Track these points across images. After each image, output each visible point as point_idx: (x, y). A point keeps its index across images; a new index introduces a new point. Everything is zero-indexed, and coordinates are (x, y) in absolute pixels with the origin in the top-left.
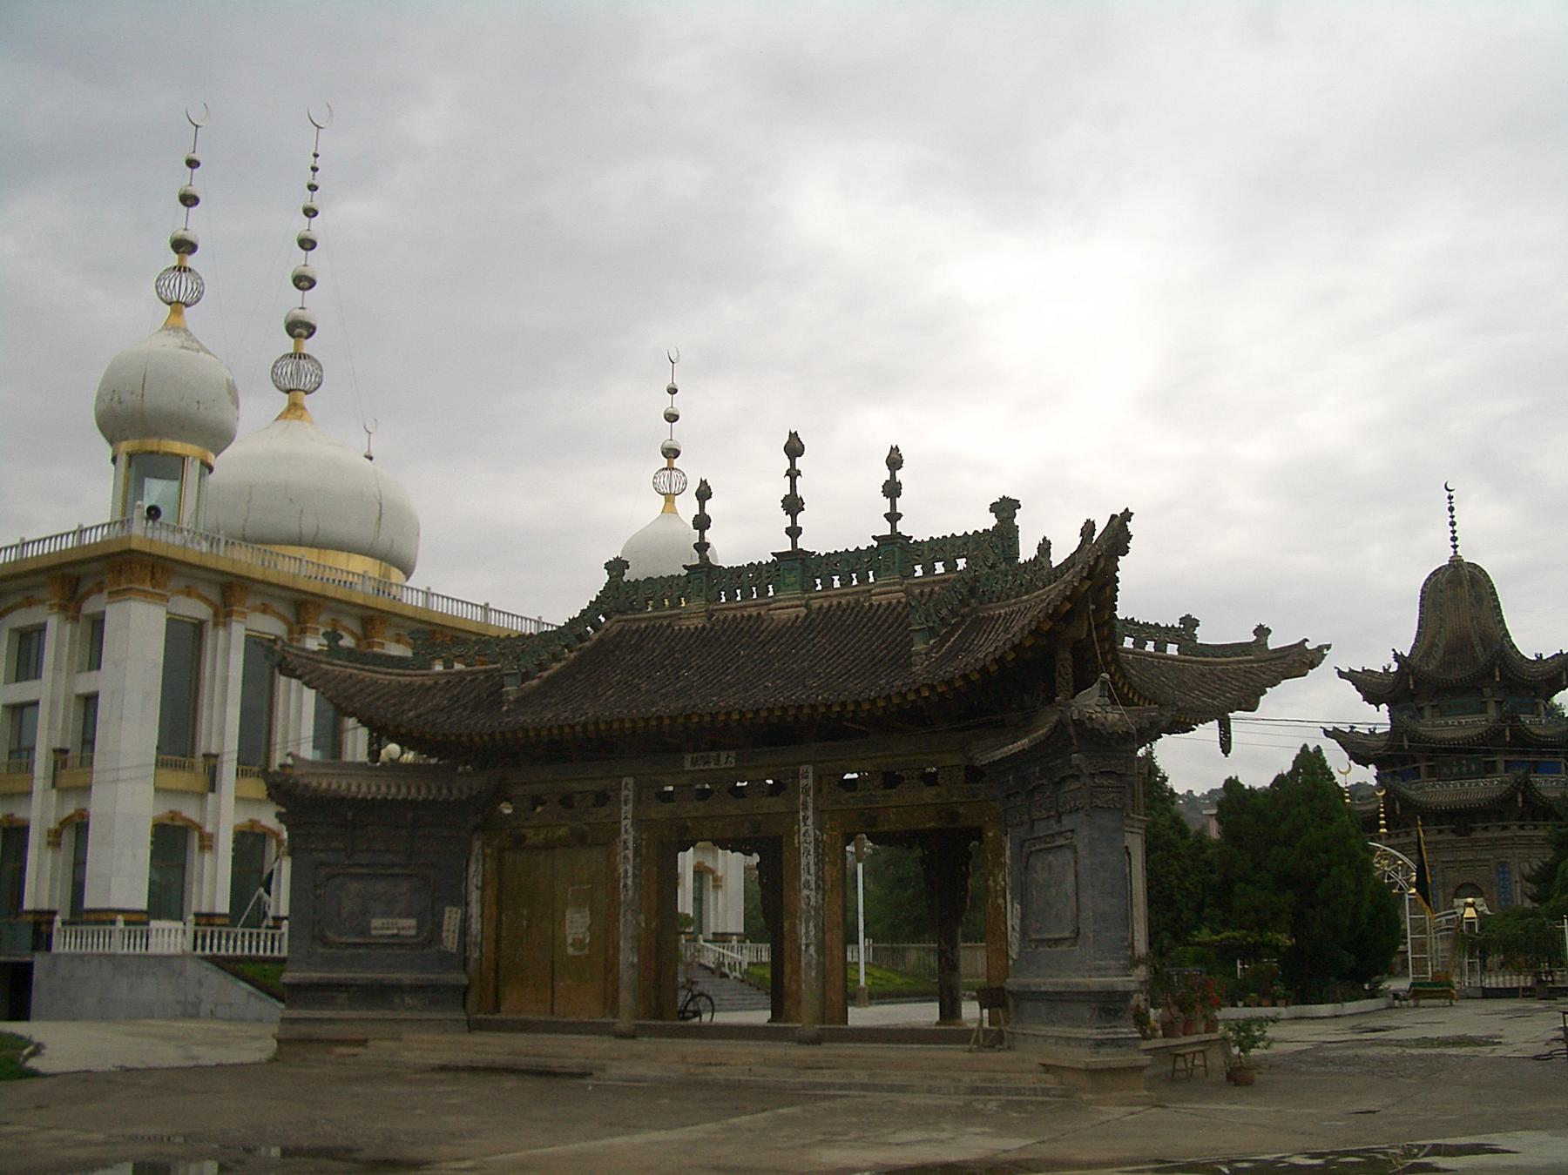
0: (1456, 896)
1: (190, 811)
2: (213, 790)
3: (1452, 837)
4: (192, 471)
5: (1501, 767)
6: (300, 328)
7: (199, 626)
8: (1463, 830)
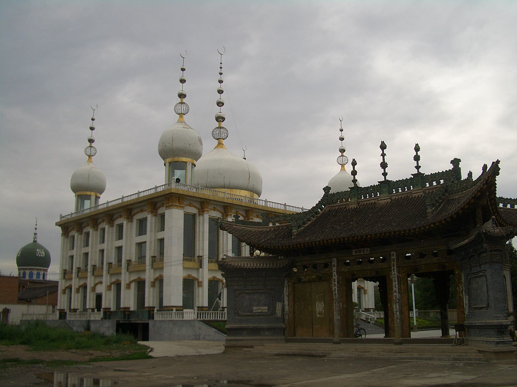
1: (194, 274)
2: (201, 268)
4: (189, 167)
6: (220, 119)
7: (194, 215)
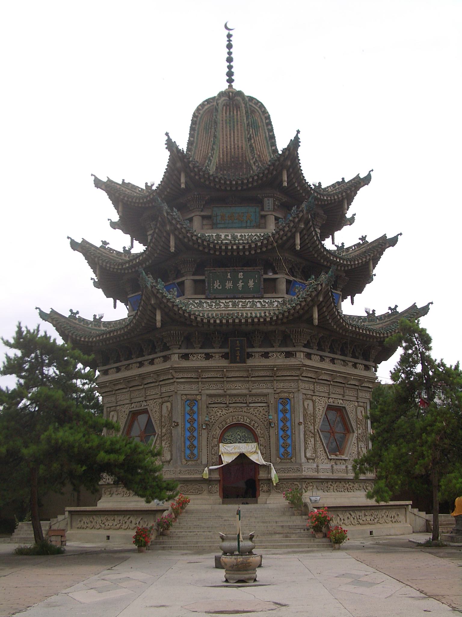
0: (222, 439)
3: (224, 363)
5: (283, 286)
8: (236, 356)
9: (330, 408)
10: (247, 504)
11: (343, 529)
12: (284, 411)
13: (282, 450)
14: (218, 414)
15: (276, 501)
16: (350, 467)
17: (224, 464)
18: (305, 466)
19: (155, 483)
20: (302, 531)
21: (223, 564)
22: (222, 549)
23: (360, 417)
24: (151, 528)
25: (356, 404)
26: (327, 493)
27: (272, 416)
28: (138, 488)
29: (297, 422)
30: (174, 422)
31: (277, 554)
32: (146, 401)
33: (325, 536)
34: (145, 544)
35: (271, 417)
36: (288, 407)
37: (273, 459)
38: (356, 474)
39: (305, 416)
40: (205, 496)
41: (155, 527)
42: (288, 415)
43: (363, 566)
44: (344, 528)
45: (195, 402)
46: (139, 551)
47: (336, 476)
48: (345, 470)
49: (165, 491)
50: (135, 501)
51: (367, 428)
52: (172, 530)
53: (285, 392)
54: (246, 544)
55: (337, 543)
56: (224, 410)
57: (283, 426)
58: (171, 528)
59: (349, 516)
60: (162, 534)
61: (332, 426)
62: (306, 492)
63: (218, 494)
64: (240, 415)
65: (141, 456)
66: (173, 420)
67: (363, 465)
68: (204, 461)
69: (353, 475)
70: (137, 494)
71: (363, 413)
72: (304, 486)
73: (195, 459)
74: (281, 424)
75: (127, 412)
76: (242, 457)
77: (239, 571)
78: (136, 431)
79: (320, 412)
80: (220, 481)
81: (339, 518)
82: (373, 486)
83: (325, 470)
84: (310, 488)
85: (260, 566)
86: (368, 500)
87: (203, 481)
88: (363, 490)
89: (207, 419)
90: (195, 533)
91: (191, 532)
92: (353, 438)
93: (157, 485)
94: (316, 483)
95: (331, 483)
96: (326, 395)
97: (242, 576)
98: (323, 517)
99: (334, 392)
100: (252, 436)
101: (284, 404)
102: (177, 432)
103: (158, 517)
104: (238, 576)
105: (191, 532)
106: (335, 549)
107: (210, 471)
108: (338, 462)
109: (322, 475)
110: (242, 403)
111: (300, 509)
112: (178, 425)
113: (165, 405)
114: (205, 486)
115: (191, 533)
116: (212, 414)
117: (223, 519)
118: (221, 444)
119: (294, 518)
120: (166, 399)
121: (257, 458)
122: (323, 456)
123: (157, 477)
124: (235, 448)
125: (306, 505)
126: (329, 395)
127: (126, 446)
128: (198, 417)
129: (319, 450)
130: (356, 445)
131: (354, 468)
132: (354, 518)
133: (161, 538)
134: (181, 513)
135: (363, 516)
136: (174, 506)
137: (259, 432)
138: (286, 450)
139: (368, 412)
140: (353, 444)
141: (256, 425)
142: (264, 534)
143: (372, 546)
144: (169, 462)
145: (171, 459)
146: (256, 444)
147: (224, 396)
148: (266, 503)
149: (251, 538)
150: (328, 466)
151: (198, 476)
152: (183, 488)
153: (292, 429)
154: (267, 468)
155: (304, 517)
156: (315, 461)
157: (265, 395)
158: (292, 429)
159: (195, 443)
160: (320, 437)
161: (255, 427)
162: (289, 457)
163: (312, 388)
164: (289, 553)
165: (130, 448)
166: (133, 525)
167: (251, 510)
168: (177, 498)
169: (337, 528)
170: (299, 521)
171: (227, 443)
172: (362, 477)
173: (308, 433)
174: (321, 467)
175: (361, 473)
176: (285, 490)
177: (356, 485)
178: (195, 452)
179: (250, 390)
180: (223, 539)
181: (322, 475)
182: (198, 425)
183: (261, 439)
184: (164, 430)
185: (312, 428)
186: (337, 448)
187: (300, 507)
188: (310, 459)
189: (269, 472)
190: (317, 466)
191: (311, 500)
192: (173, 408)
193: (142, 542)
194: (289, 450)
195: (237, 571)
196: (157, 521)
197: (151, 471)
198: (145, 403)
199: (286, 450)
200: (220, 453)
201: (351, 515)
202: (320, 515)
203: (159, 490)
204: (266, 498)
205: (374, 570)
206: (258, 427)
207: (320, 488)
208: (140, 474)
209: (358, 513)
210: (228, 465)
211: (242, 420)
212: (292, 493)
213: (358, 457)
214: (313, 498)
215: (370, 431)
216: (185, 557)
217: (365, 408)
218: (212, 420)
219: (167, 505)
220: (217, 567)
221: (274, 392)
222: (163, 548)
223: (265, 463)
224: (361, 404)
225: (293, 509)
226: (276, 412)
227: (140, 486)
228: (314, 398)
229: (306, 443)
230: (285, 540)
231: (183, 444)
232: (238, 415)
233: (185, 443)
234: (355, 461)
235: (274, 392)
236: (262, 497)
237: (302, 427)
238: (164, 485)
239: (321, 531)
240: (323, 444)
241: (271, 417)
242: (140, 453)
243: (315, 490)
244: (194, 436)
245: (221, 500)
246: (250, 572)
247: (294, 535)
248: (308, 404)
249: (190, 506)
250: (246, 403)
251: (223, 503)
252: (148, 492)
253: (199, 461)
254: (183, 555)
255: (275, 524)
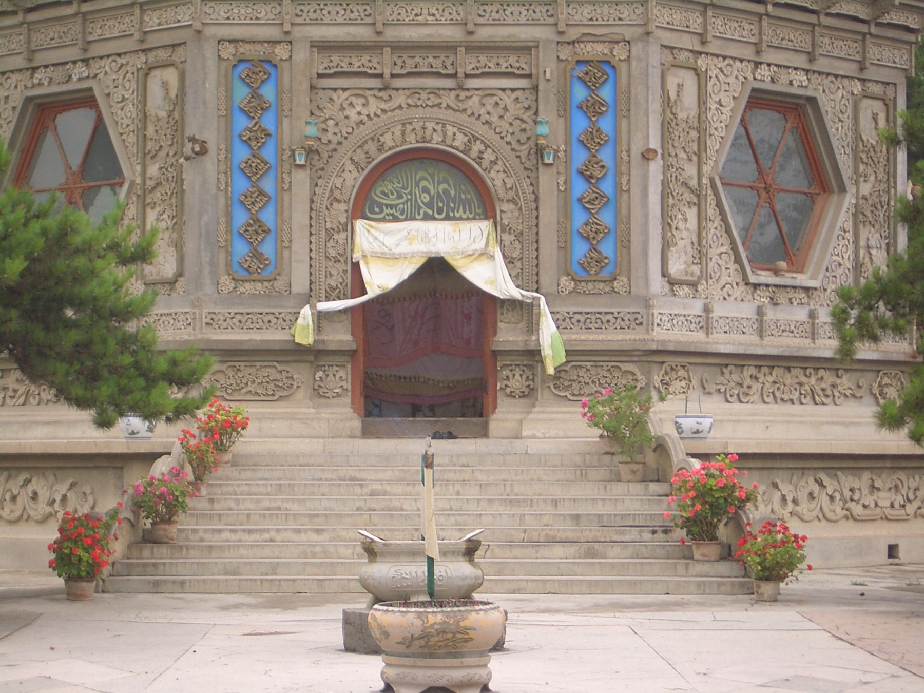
0: (364, 205)
9: (759, 100)
10: (451, 436)
11: (792, 531)
12: (593, 108)
13: (580, 249)
14: (352, 113)
15: (547, 432)
16: (824, 316)
17: (372, 292)
18: (663, 308)
19: (127, 359)
20: (647, 536)
21: (376, 633)
22: (370, 592)
23: (870, 135)
24: (114, 515)
25: (857, 88)
26: (737, 406)
27: (549, 127)
28: (67, 374)
29: (636, 151)
30: (192, 139)
31: (557, 611)
32: (85, 61)
33: (727, 554)
34: (92, 572)
35: (542, 130)
36: (606, 93)
37: (547, 280)
38: (843, 339)
39: (666, 128)
40: (301, 406)
41: (126, 514)
42: (606, 124)
43: (859, 656)
44: (796, 527)
45: (268, 67)
46: (72, 596)
47: (773, 345)
48: (802, 324)
49: (163, 385)
50: (48, 423)
51: (891, 176)
52: (183, 522)
53: (597, 39)
54: (455, 571)
55: (767, 579)
56: (372, 100)
57: (589, 164)
58: (181, 517)
59: (816, 488)
60: (149, 539)
61: (765, 164)
62: (662, 399)
63: (348, 400)
64: (430, 119)
65: (80, 262)
66: (189, 132)
67: (870, 308)
68: (300, 284)
69: (835, 343)
70: (65, 395)
71: (882, 123)
72: (657, 379)
73: (266, 274)
74: (580, 157)
75: (17, 100)
76: (436, 269)
77: (432, 656)
78: (50, 171)
79: (724, 117)
80: (353, 353)
81: (777, 496)
82: (907, 384)
83: (735, 325)
84: (677, 385)
85: (499, 647)
86: (885, 432)
87: (296, 353)
88: (868, 399)
89: (312, 131)
90: (266, 536)
91: (250, 531)
92: (839, 214)
93: (136, 365)
94: (700, 369)
95: (752, 371)
96: (748, 52)
97: (440, 673)
98: (723, 489)
99: (776, 42)
100: (475, 196)
101: (591, 83)
102: (201, 178)
103: (135, 478)
104: (430, 673)
105: (250, 531)
106: (761, 600)
107: (321, 318)
108: (782, 297)
109: (723, 342)
110: (438, 75)
111: (639, 458)
112: (204, 151)
113: (156, 77)
114: (300, 373)
115: (256, 536)
116: (328, 113)
117: (366, 490)
118: (360, 224)
119: (618, 489)
120: (162, 55)
121: (490, 276)
122: (728, 273)
123: (134, 338)
124: (409, 238)
125: (661, 447)
126: (758, 52)
127: (25, 225)
128: (279, 123)
129: (713, 252)
130: (849, 236)
131: (840, 318)
132: (832, 498)
133: (146, 553)
134: (216, 464)
135: (865, 491)
136: (193, 442)
137: (499, 183)
138: (594, 248)
139: (900, 121)
140: (837, 232)
141: (489, 156)
142: (510, 544)
143: (894, 594)
144: (171, 283)
145: (179, 274)
146: (485, 226)
147: (375, 47)
148: (518, 437)
149: (471, 550)
150: (747, 310)
151: (274, 336)
152: (220, 377)
153: (618, 174)
154: (525, 312)
155: (654, 487)
156: (693, 287)
157: (526, 49)
158: (618, 174)
159: (268, 217)
160: (719, 205)
161: (485, 163)
162: (604, 274)
163: (696, 27)
164: (597, 608)
165: (44, 232)
166: (42, 508)
167: (463, 460)
168: (201, 414)
169: (769, 526)
170: (635, 500)
171: (383, 220)
172: (865, 351)
173: (676, 189)
174: (719, 311)
175: (862, 337)
176: (587, 390)
177: (846, 382)
178: (268, 249)
179: (471, 27)
180: (371, 552)
181: (724, 342)
182: (280, 151)
183: (506, 207)
184: (153, 170)
185: (691, 170)
186: (779, 247)
187: (641, 452)
188: (681, 283)
189: (533, 326)
190: (707, 309)
191: (678, 427)
192: (189, 90)
193: (80, 564)
194: (607, 248)
195: (424, 656)
196: (131, 491)
197: (113, 314)
198: (80, 70)
199: (594, 248)
200: (357, 256)
201: (821, 485)
202: (712, 482)
203: (141, 382)
204: (519, 416)
205: (895, 670)
206: (494, 163)
207: (712, 387)
208: (74, 325)
209: (848, 481)
210: (386, 299)
211: (437, 138)
212: (612, 400)
213: (856, 281)
214: (688, 424)
215: (905, 188)
216: (235, 617)
217: (889, 105)
218: (330, 136)
219: (165, 435)
220: (349, 648)
221: (558, 38)
222: (156, 588)
223: (516, 293)
224: (877, 89)
225: (617, 458)
226: (564, 110)
227: (77, 366)
228: (702, 62)
229: (667, 223)
230: (586, 563)
231: (223, 220)
232: (425, 119)
233: (229, 215)
234: (844, 295)
235: (558, 38)
236: (504, 415)
237: (655, 167)
238: (162, 365)
239: (713, 538)
240: (728, 231)
241: (542, 130)
242: (77, 251)
243: (694, 394)
244: (261, 193)
245: (356, 424)
246: (467, 661)
247: (617, 549)
248: (680, 86)
249: (247, 443)
250: (455, 76)
251: (366, 433)
252: (105, 390)
253: (279, 284)
254: (225, 608)
255: (549, 510)
